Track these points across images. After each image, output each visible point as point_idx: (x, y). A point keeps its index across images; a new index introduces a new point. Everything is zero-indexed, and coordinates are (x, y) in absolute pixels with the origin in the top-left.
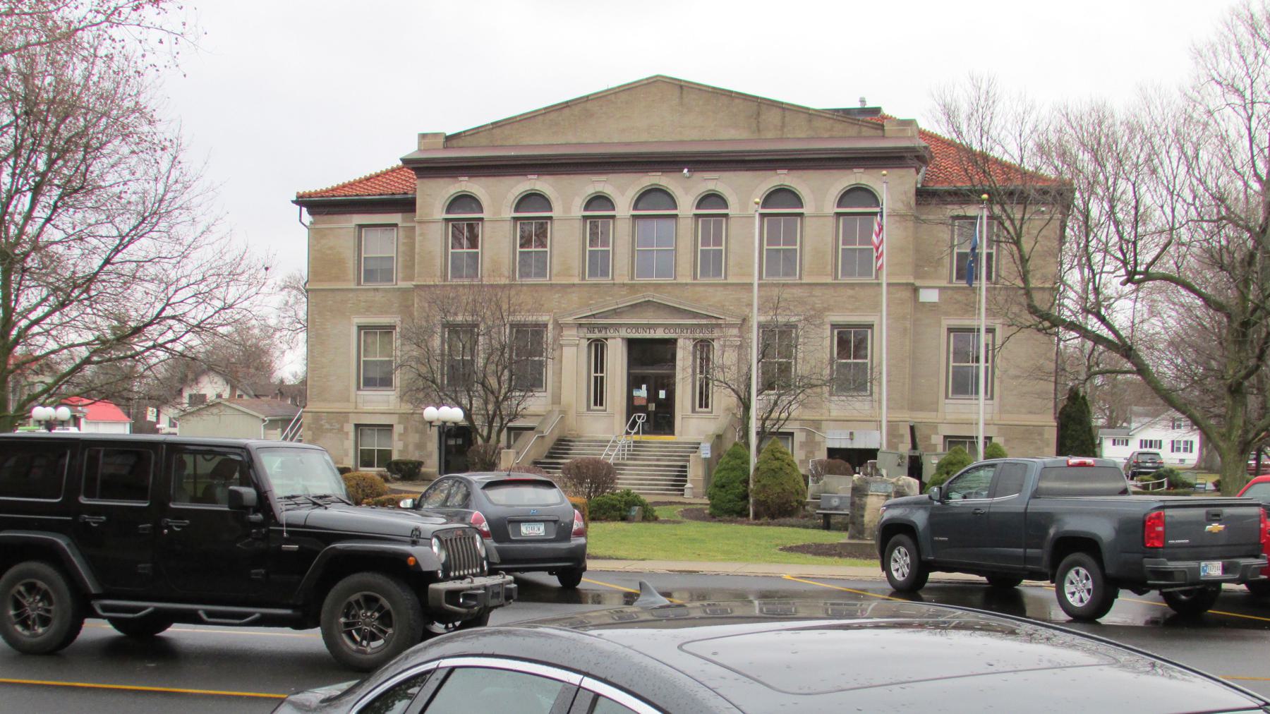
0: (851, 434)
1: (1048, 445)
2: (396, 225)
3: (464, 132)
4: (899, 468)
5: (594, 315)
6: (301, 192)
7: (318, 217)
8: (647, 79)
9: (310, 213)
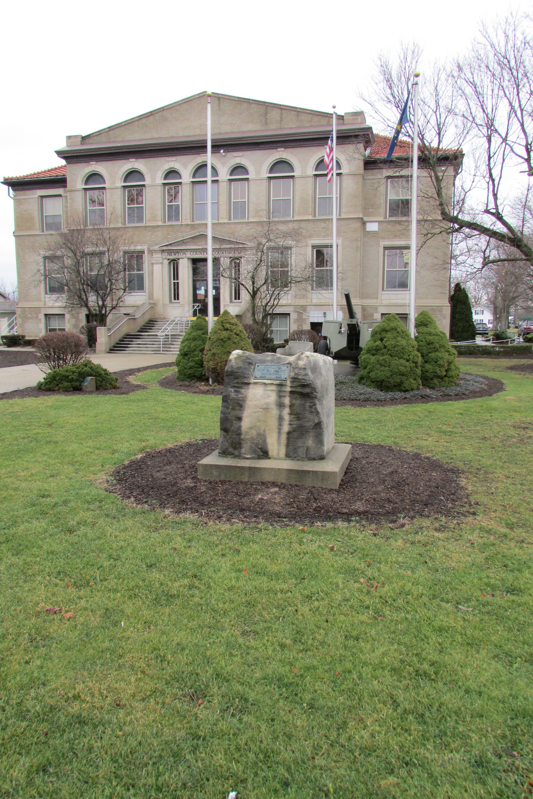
0: (325, 313)
1: (445, 318)
2: (60, 196)
3: (93, 134)
4: (339, 335)
5: (170, 244)
6: (7, 177)
7: (18, 192)
8: (198, 94)
9: (14, 190)
